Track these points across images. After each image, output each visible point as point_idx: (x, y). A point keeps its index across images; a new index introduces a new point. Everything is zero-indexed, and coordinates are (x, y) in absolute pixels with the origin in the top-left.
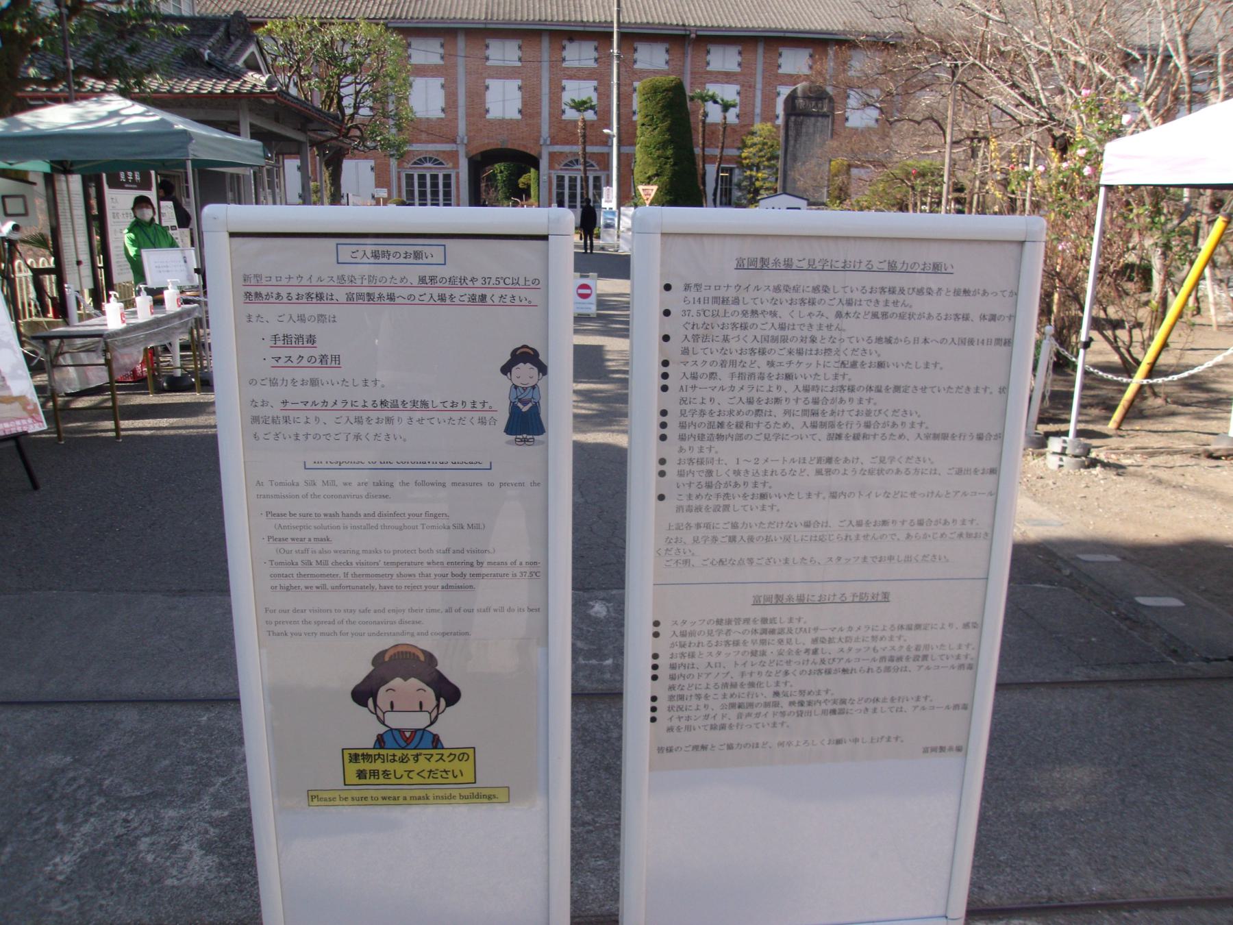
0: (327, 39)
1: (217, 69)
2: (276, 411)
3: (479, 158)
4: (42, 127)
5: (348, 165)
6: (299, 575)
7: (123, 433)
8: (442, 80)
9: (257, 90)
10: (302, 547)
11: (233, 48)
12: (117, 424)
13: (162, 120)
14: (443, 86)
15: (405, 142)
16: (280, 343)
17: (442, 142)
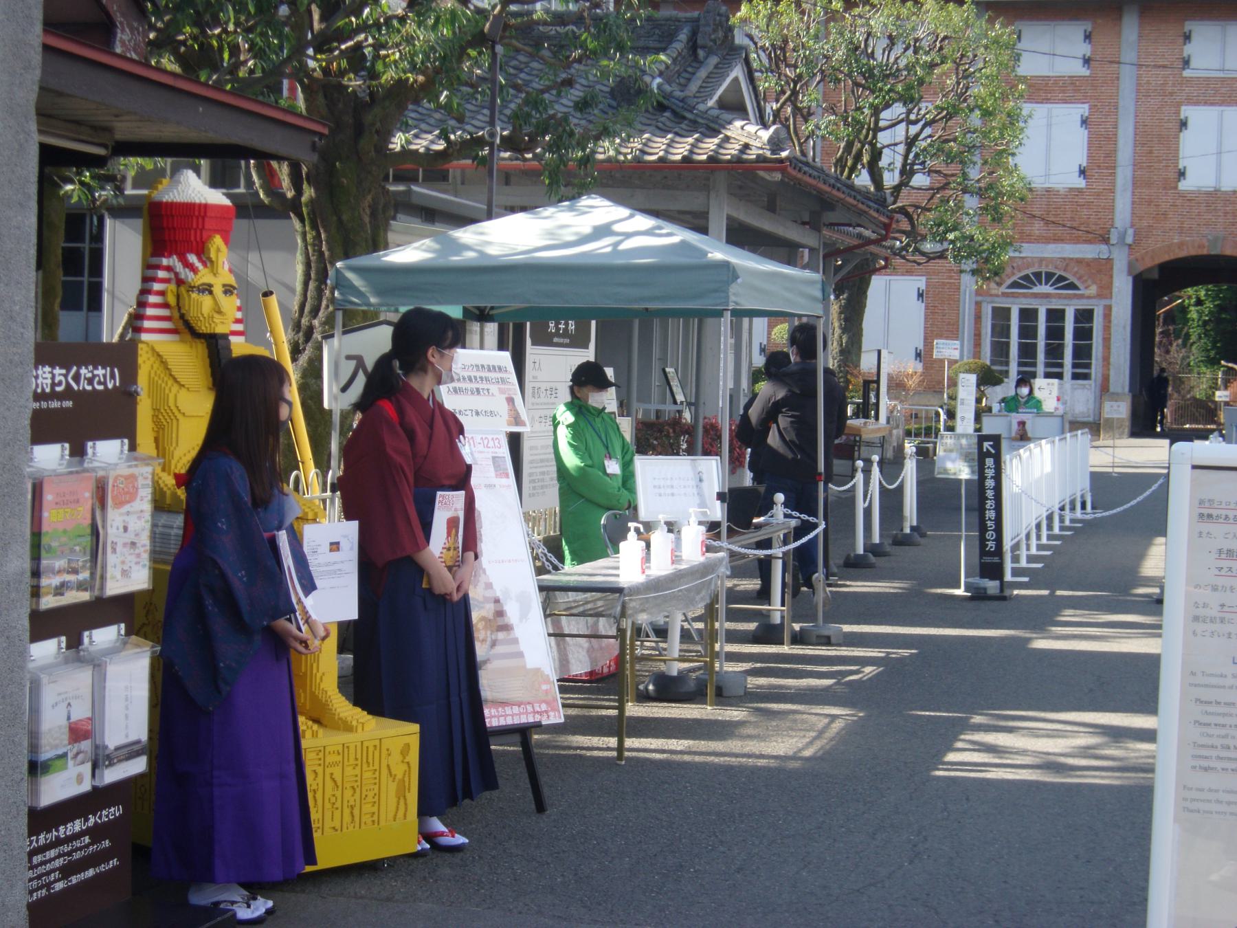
0: (860, 36)
1: (675, 114)
2: (1214, 612)
3: (1156, 276)
4: (492, 251)
5: (877, 284)
6: (1219, 758)
7: (627, 754)
8: (1084, 109)
9: (752, 155)
10: (1223, 732)
11: (702, 73)
12: (621, 743)
13: (683, 244)
14: (1084, 122)
15: (1005, 244)
16: (1223, 556)
17: (1077, 240)
